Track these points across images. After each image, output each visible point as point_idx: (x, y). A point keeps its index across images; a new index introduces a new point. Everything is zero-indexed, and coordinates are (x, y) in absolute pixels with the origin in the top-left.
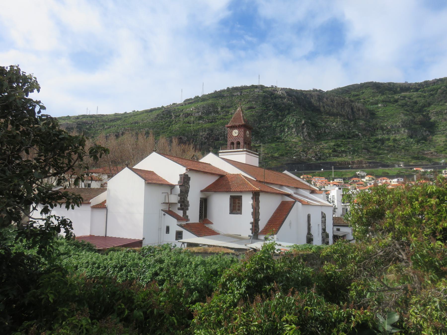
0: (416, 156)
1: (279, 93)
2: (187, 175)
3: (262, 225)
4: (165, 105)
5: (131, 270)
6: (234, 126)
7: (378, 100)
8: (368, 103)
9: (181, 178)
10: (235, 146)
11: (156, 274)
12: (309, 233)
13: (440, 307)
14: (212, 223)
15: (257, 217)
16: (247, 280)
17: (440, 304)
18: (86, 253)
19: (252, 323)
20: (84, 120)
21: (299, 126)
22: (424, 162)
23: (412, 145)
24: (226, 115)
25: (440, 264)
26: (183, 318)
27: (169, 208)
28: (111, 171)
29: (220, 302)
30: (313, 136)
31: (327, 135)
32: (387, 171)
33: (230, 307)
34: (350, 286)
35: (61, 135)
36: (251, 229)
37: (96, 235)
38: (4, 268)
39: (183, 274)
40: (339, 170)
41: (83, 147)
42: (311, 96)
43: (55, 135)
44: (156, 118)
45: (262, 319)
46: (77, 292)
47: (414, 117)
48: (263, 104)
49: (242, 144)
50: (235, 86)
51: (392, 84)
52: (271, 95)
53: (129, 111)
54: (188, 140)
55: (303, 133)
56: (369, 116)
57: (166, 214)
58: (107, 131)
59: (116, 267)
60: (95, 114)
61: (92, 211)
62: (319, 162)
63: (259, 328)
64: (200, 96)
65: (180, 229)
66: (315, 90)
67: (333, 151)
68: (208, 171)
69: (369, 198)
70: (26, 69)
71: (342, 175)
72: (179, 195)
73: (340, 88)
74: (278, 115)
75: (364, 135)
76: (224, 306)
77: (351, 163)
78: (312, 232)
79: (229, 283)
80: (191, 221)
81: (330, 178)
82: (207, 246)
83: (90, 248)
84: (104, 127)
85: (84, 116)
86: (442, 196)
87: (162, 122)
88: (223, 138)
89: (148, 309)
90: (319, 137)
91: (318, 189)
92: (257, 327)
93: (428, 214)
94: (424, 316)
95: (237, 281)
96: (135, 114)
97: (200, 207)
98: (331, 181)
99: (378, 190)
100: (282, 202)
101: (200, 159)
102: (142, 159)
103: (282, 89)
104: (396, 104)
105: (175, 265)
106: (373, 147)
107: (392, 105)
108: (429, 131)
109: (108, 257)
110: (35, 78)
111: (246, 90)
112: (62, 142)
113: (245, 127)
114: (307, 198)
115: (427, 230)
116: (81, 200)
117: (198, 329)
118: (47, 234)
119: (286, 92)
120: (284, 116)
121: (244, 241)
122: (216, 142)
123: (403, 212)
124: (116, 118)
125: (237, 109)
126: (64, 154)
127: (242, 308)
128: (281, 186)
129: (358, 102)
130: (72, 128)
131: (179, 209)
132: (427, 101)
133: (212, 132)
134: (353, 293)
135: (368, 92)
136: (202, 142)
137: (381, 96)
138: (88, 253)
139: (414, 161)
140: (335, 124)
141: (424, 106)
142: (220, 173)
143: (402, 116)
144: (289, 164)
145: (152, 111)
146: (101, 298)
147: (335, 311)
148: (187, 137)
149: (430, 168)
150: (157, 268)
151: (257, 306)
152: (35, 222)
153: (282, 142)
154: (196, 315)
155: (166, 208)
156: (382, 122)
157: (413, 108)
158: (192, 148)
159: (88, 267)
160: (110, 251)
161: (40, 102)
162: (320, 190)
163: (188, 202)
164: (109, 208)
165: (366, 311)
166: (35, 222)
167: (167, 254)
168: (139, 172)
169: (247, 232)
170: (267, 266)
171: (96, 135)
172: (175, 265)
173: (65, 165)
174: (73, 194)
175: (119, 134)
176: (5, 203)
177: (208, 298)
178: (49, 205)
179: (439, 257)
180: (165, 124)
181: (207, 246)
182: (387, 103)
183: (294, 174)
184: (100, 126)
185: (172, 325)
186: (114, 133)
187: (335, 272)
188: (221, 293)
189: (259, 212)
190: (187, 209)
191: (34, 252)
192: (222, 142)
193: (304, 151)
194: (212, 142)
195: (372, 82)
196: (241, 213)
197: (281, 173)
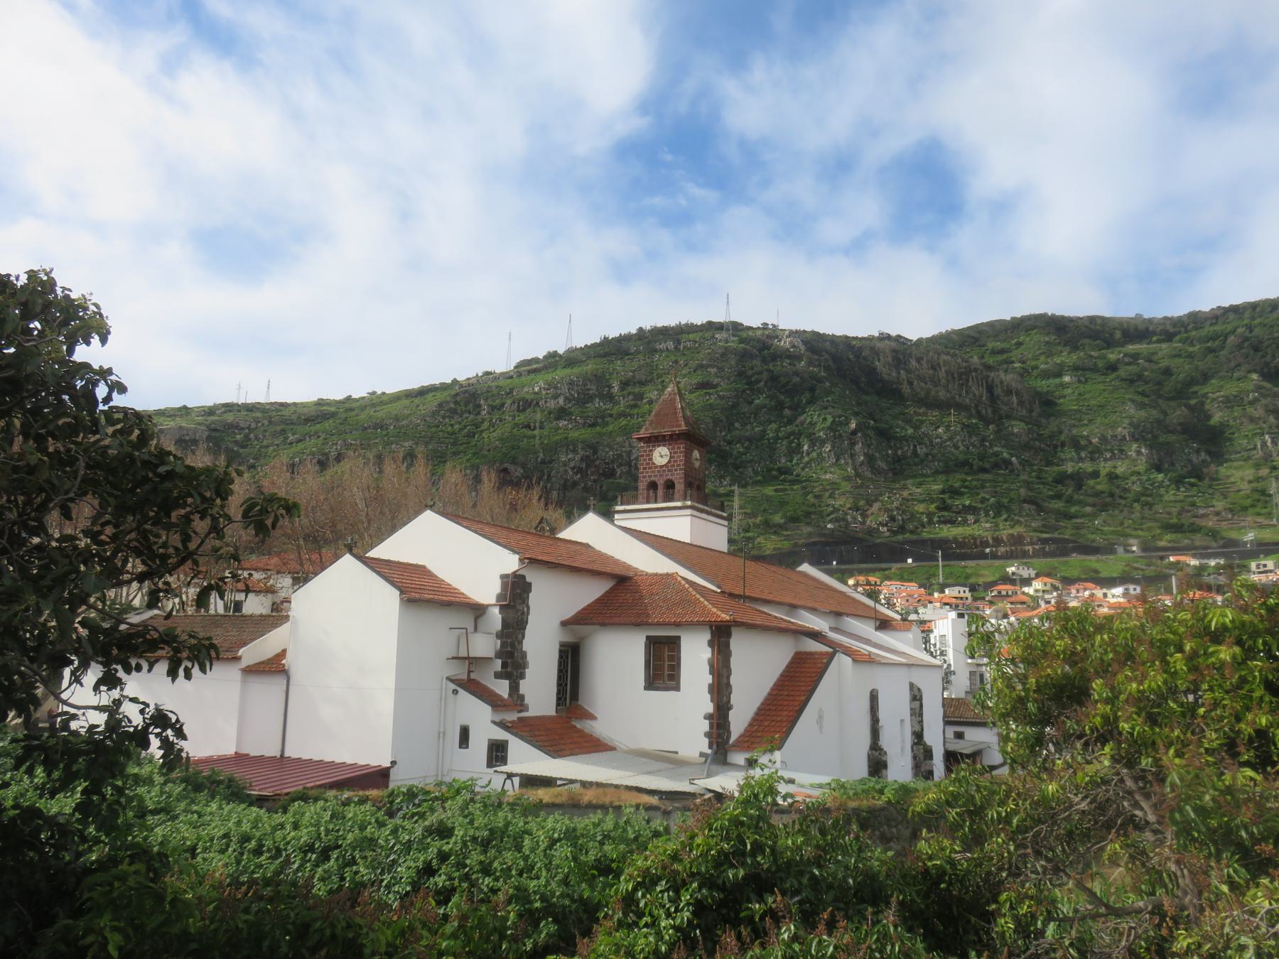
0: (1175, 521)
1: (785, 343)
2: (523, 577)
3: (739, 721)
5: (354, 858)
6: (656, 437)
7: (1061, 365)
9: (504, 586)
10: (660, 492)
11: (428, 871)
12: (875, 746)
14: (593, 718)
15: (725, 699)
16: (695, 885)
18: (220, 808)
20: (230, 418)
21: (840, 436)
22: (1198, 539)
23: (1162, 491)
24: (635, 406)
25: (1251, 835)
27: (469, 672)
28: (302, 565)
31: (922, 461)
32: (1095, 565)
34: (996, 902)
35: (163, 463)
36: (707, 735)
37: (252, 754)
39: (509, 869)
42: (876, 352)
44: (434, 414)
47: (1165, 414)
48: (741, 374)
49: (680, 486)
50: (659, 325)
51: (1099, 321)
52: (760, 351)
54: (527, 476)
55: (852, 456)
56: (1037, 410)
57: (461, 691)
58: (293, 450)
59: (311, 848)
60: (262, 401)
61: (244, 682)
62: (900, 537)
64: (561, 352)
65: (501, 735)
66: (885, 337)
67: (939, 508)
68: (582, 564)
70: (73, 281)
71: (968, 577)
73: (954, 332)
74: (781, 406)
77: (990, 540)
78: (884, 742)
79: (644, 896)
81: (931, 585)
82: (578, 786)
83: (235, 793)
84: (286, 438)
85: (229, 407)
86: (1250, 638)
91: (898, 617)
93: (1211, 689)
95: (667, 890)
96: (376, 401)
97: (560, 671)
98: (936, 595)
99: (1067, 619)
100: (797, 654)
101: (561, 530)
102: (393, 529)
104: (1113, 376)
105: (485, 845)
106: (1052, 497)
107: (1101, 378)
108: (1209, 452)
109: (289, 818)
110: (96, 305)
111: (691, 336)
112: (167, 485)
113: (690, 438)
114: (868, 642)
118: (113, 748)
120: (798, 409)
123: (1141, 683)
125: (665, 387)
126: (170, 517)
128: (793, 607)
130: (195, 442)
131: (498, 676)
133: (595, 452)
134: (1005, 924)
135: (1033, 342)
136: (566, 480)
138: (227, 808)
139: (1169, 537)
140: (944, 431)
141: (1192, 382)
142: (617, 571)
143: (1131, 409)
144: (814, 543)
145: (423, 392)
146: (266, 944)
149: (1215, 555)
150: (432, 852)
152: (74, 717)
153: (793, 482)
156: (1074, 426)
157: (1157, 386)
160: (294, 800)
161: (110, 371)
162: (904, 620)
163: (524, 655)
164: (293, 673)
166: (74, 717)
167: (462, 810)
168: (386, 570)
169: (695, 742)
171: (262, 461)
172: (485, 845)
174: (191, 636)
178: (119, 667)
179: (1249, 815)
180: (461, 430)
183: (830, 573)
186: (313, 454)
187: (952, 863)
188: (620, 925)
189: (728, 685)
190: (522, 676)
191: (63, 805)
192: (622, 481)
194: (595, 481)
195: (1043, 316)
196: (677, 688)
197: (793, 569)
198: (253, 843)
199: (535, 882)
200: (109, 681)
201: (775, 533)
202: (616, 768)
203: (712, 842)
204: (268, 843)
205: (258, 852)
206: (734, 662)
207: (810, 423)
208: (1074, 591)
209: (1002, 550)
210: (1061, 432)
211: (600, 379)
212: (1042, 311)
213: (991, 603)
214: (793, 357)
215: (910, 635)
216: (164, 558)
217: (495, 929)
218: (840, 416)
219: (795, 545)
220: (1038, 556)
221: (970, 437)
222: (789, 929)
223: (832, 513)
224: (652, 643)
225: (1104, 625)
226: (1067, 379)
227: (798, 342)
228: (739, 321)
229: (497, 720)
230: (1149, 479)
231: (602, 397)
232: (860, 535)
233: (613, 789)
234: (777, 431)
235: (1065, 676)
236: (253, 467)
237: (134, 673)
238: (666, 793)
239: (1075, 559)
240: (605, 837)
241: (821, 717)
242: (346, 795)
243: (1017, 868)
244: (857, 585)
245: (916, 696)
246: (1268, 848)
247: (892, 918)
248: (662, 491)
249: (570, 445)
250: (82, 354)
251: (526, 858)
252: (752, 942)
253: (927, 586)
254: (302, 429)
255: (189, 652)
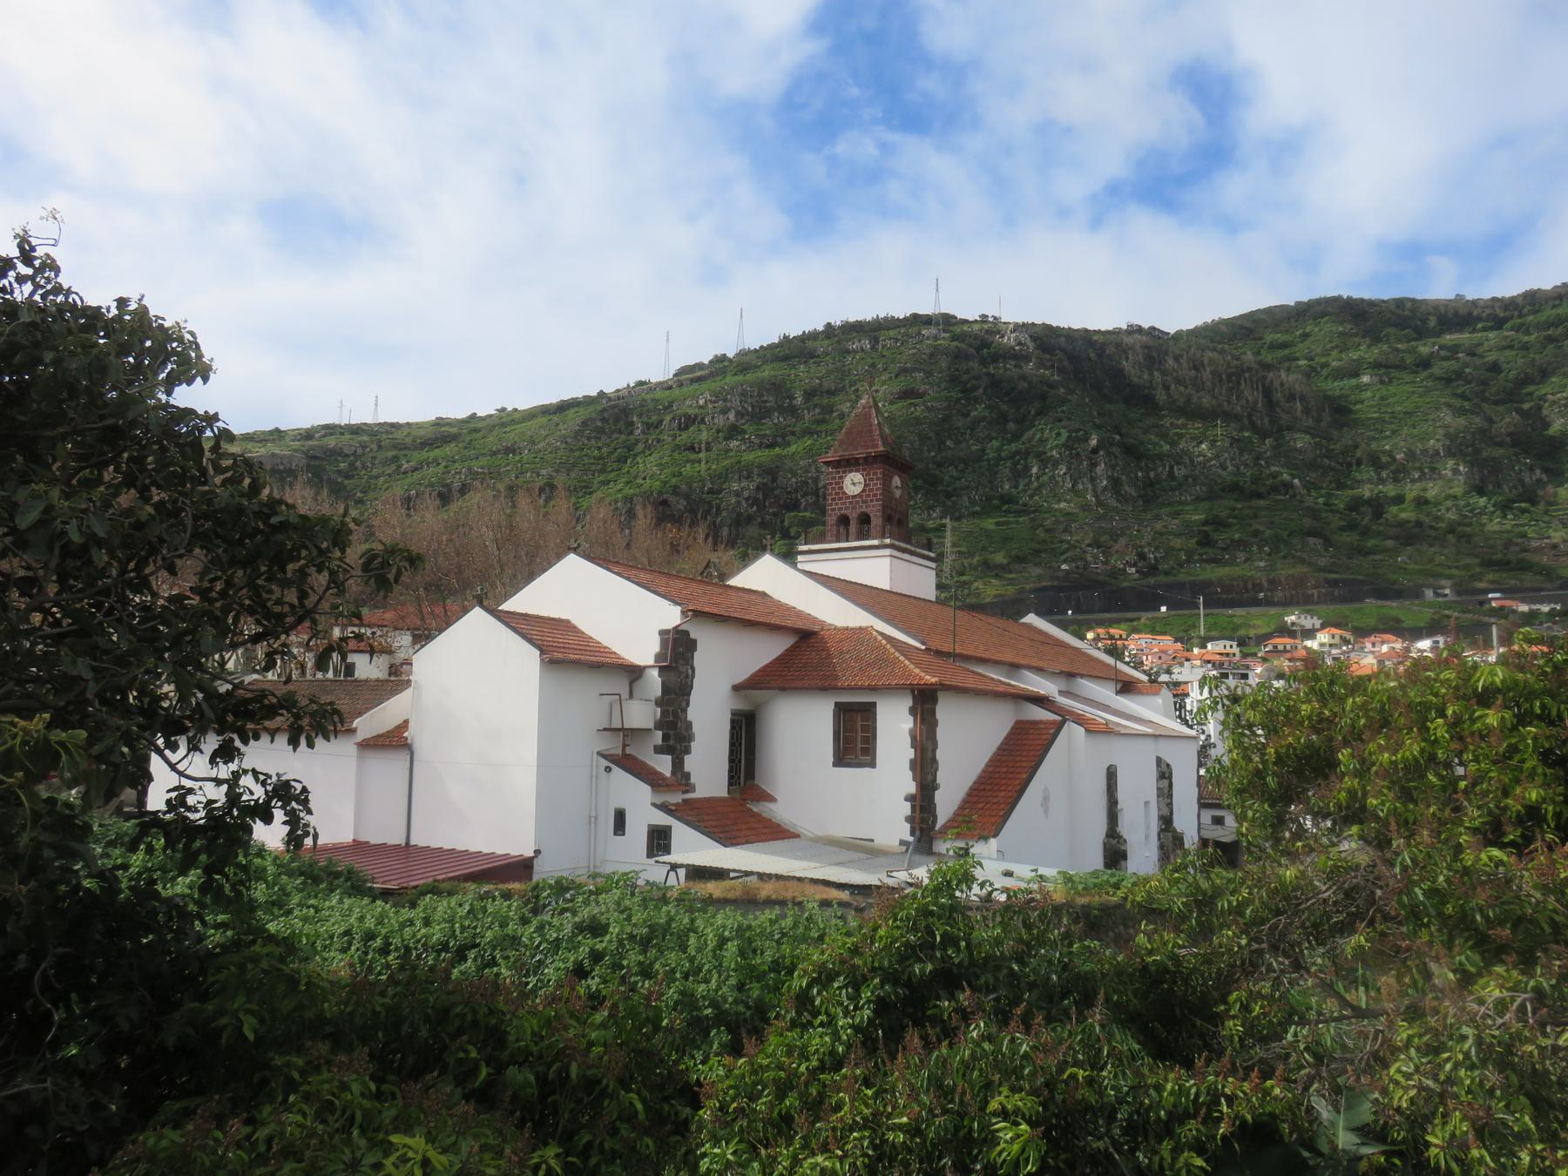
0: (1499, 556)
1: (1009, 340)
2: (687, 633)
3: (947, 802)
4: (609, 389)
5: (494, 958)
6: (848, 460)
7: (1360, 361)
8: (1325, 372)
9: (664, 643)
10: (853, 528)
11: (580, 972)
12: (1113, 833)
13: (1478, 1054)
14: (772, 799)
15: (930, 778)
16: (877, 981)
17: (1479, 1042)
18: (341, 901)
19: (888, 1118)
20: (331, 442)
21: (1078, 454)
22: (1529, 579)
23: (1484, 519)
24: (823, 421)
25: (1486, 917)
26: (666, 1099)
27: (624, 746)
28: (423, 619)
29: (789, 1053)
30: (1129, 490)
31: (1180, 485)
32: (1394, 613)
33: (822, 1068)
34: (1225, 1002)
35: (275, 513)
36: (909, 819)
37: (373, 842)
38: (97, 936)
39: (673, 971)
40: (1224, 611)
41: (343, 551)
42: (1122, 349)
43: (258, 515)
44: (577, 434)
45: (921, 1104)
46: (329, 1008)
47: (1490, 421)
48: (954, 380)
49: (876, 521)
50: (852, 319)
51: (1408, 305)
52: (978, 349)
53: (485, 409)
54: (692, 511)
55: (1093, 480)
56: (1327, 418)
57: (615, 769)
58: (409, 480)
59: (445, 947)
60: (369, 421)
61: (360, 758)
62: (1152, 581)
63: (913, 1137)
64: (731, 355)
65: (662, 819)
66: (1135, 330)
67: (1199, 543)
68: (758, 617)
69: (1288, 707)
70: (167, 309)
71: (1236, 628)
72: (659, 703)
73: (1223, 322)
74: (1003, 419)
75: (1310, 486)
76: (803, 1069)
77: (1265, 584)
78: (1124, 828)
79: (819, 993)
80: (700, 793)
81: (1190, 639)
82: (754, 878)
83: (357, 886)
84: (399, 467)
85: (330, 429)
86: (1526, 700)
87: (599, 448)
88: (811, 499)
89: (549, 1066)
90: (1151, 494)
91: (1145, 678)
92: (905, 1132)
93: (1476, 760)
94: (1430, 1083)
95: (846, 986)
96: (506, 419)
97: (732, 744)
98: (1196, 651)
99: (1317, 679)
100: (1017, 723)
101: (732, 575)
102: (531, 577)
103: (1020, 327)
104: (1424, 374)
105: (645, 944)
106: (1342, 529)
107: (1409, 378)
108: (1546, 470)
109: (418, 914)
110: (192, 334)
111: (892, 333)
112: (279, 537)
113: (889, 461)
114: (1106, 708)
115: (1474, 815)
116: (336, 719)
117: (716, 1141)
118: (226, 831)
119: (1034, 338)
120: (1024, 422)
121: (882, 860)
122: (788, 516)
123: (1395, 752)
124: (442, 434)
125: (859, 398)
126: (285, 572)
127: (858, 1072)
128: (1014, 667)
129: (1288, 370)
130: (291, 472)
131: (659, 750)
132: (1533, 360)
133: (774, 479)
134: (1234, 1027)
135: (1324, 331)
136: (739, 514)
137: (1369, 346)
138: (347, 902)
139: (1491, 576)
140: (1207, 448)
141: (1526, 380)
142: (800, 625)
143: (1447, 417)
144: (1045, 589)
145: (563, 407)
146: (406, 1029)
147: (1172, 1084)
148: (687, 497)
149: (1548, 600)
150: (584, 951)
151: (908, 1067)
152: (191, 791)
153: (1019, 513)
154: (709, 1097)
155: (614, 745)
156: (1374, 439)
157: (1481, 387)
158: (702, 536)
159: (349, 948)
160: (424, 894)
161: (215, 418)
162: (1152, 681)
163: (689, 725)
164: (417, 747)
165: (1269, 1083)
166: (191, 791)
167: (618, 904)
168: (522, 625)
169: (894, 828)
170: (944, 935)
171: (371, 495)
172: (645, 944)
173: (286, 609)
174: (312, 701)
175: (450, 491)
176: (118, 729)
177: (749, 1044)
178: (235, 736)
179: (1484, 896)
180: (610, 453)
181: (754, 878)
182: (1394, 373)
183: (1063, 625)
184: (386, 462)
185: (630, 1117)
186: (431, 485)
187: (1174, 958)
188: (794, 1024)
189: (934, 761)
190: (687, 751)
191: (182, 886)
192: (808, 514)
193: (1096, 544)
194: (774, 514)
195: (1336, 300)
196: (872, 764)
197: (1016, 620)
198: (379, 941)
199: (703, 986)
200: (225, 753)
201: (996, 576)
202: (801, 858)
203: (897, 933)
204: (396, 941)
205: (384, 950)
206: (941, 733)
207: (1041, 440)
208: (1368, 645)
209: (1279, 595)
210: (1356, 447)
211: (777, 387)
212: (1335, 294)
213: (1264, 660)
214: (1019, 357)
215: (1159, 700)
216: (280, 617)
217: (648, 1019)
218: (1077, 430)
219: (1022, 591)
220: (1325, 602)
221: (1241, 454)
222: (978, 1026)
223: (1067, 550)
224: (842, 711)
225: (1359, 685)
226: (1366, 379)
227: (1025, 337)
228: (952, 312)
229: (658, 802)
230: (1468, 504)
231: (782, 410)
232: (1102, 578)
233: (796, 882)
234: (999, 450)
235: (1310, 745)
236: (361, 501)
237: (252, 742)
238: (858, 887)
239: (1370, 603)
240: (784, 935)
241: (1046, 800)
242: (486, 888)
243: (1251, 964)
244: (1097, 639)
245: (1165, 773)
246: (1505, 932)
247: (1098, 1017)
248: (854, 527)
249: (745, 472)
250: (183, 396)
251: (692, 960)
252: (940, 1041)
253: (1185, 640)
254: (418, 456)
255: (315, 721)
